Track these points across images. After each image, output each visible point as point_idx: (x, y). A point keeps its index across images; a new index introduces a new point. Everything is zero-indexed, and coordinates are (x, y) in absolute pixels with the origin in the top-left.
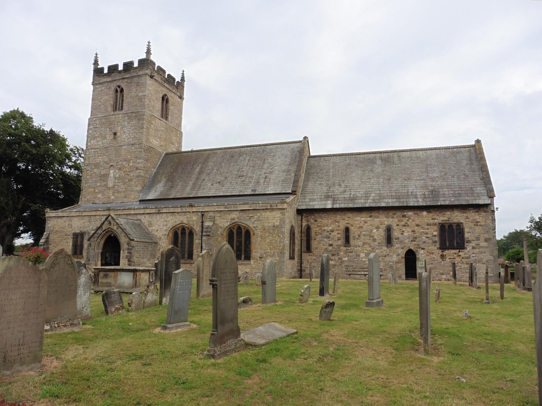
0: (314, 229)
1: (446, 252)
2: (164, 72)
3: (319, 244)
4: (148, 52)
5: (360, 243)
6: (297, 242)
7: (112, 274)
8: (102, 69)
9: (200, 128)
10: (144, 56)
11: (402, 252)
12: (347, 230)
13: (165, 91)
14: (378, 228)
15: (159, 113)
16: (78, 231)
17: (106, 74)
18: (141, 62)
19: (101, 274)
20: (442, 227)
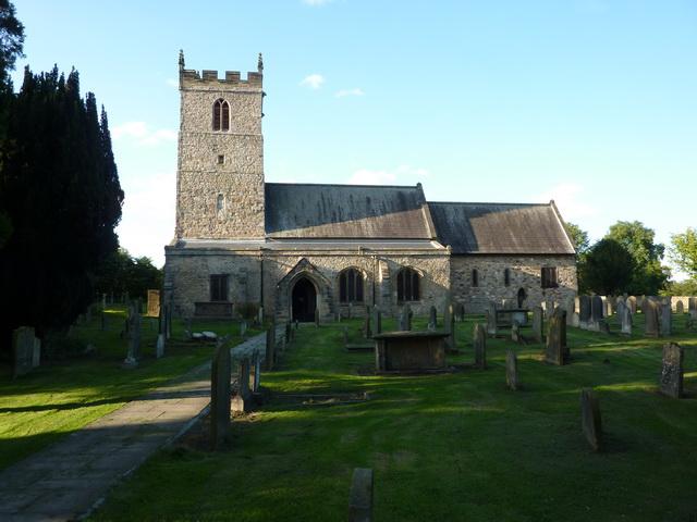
1: (546, 290)
11: (516, 290)
12: (475, 272)
14: (499, 271)
18: (251, 75)
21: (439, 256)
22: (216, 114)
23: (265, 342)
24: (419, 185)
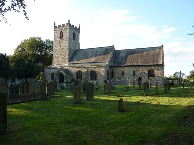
0: (114, 71)
2: (74, 26)
3: (116, 76)
4: (69, 21)
5: (126, 75)
6: (110, 75)
7: (62, 83)
8: (57, 26)
9: (85, 43)
10: (68, 22)
11: (138, 78)
12: (123, 72)
13: (74, 32)
14: (131, 71)
15: (73, 38)
16: (53, 72)
17: (66, 26)
19: (60, 83)
20: (149, 71)
21: (102, 67)
22: (60, 35)
23: (118, 105)
24: (113, 45)
